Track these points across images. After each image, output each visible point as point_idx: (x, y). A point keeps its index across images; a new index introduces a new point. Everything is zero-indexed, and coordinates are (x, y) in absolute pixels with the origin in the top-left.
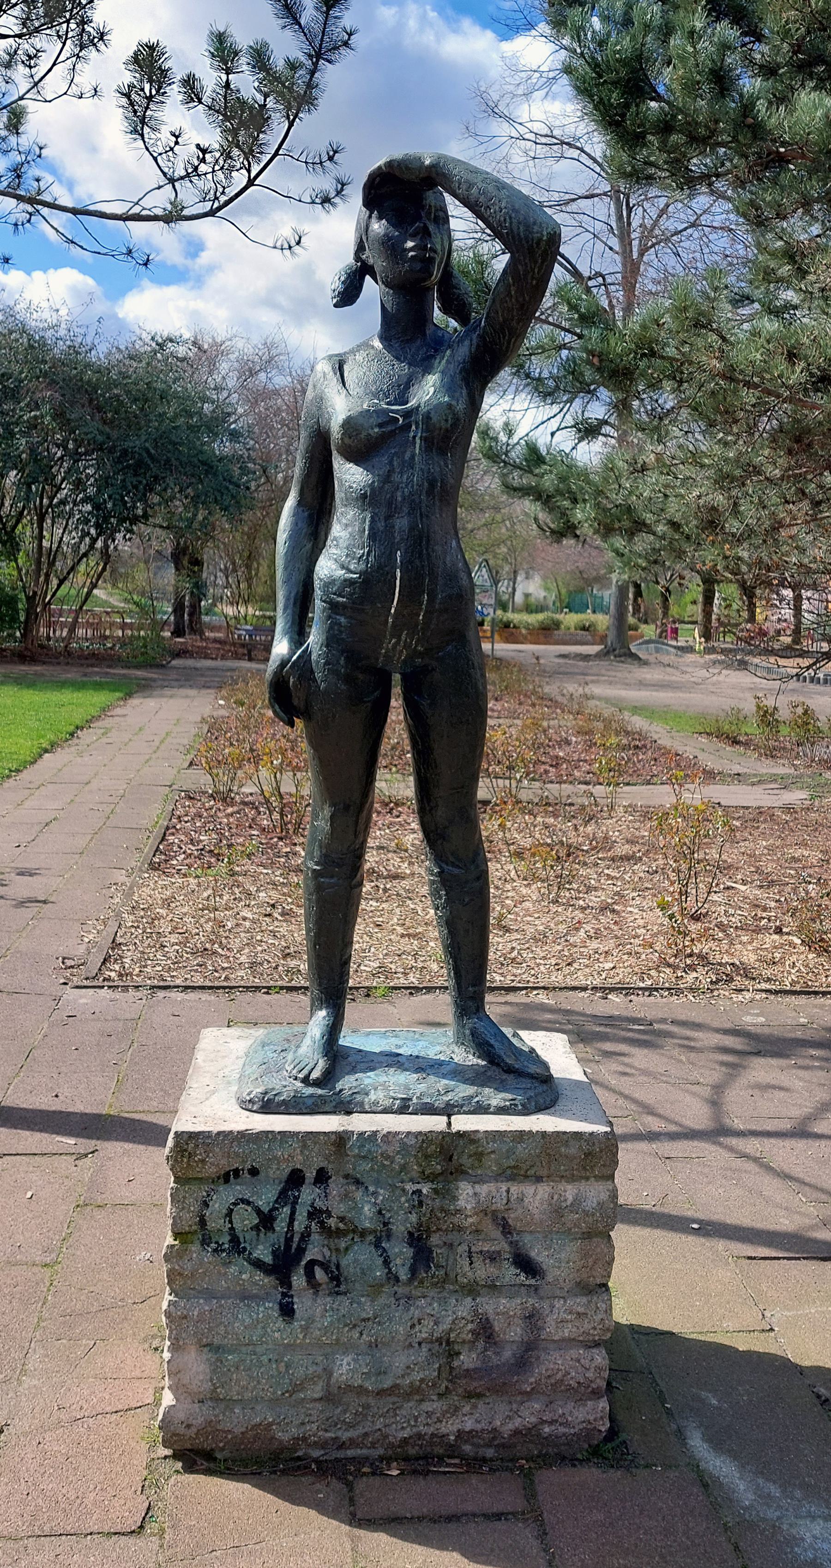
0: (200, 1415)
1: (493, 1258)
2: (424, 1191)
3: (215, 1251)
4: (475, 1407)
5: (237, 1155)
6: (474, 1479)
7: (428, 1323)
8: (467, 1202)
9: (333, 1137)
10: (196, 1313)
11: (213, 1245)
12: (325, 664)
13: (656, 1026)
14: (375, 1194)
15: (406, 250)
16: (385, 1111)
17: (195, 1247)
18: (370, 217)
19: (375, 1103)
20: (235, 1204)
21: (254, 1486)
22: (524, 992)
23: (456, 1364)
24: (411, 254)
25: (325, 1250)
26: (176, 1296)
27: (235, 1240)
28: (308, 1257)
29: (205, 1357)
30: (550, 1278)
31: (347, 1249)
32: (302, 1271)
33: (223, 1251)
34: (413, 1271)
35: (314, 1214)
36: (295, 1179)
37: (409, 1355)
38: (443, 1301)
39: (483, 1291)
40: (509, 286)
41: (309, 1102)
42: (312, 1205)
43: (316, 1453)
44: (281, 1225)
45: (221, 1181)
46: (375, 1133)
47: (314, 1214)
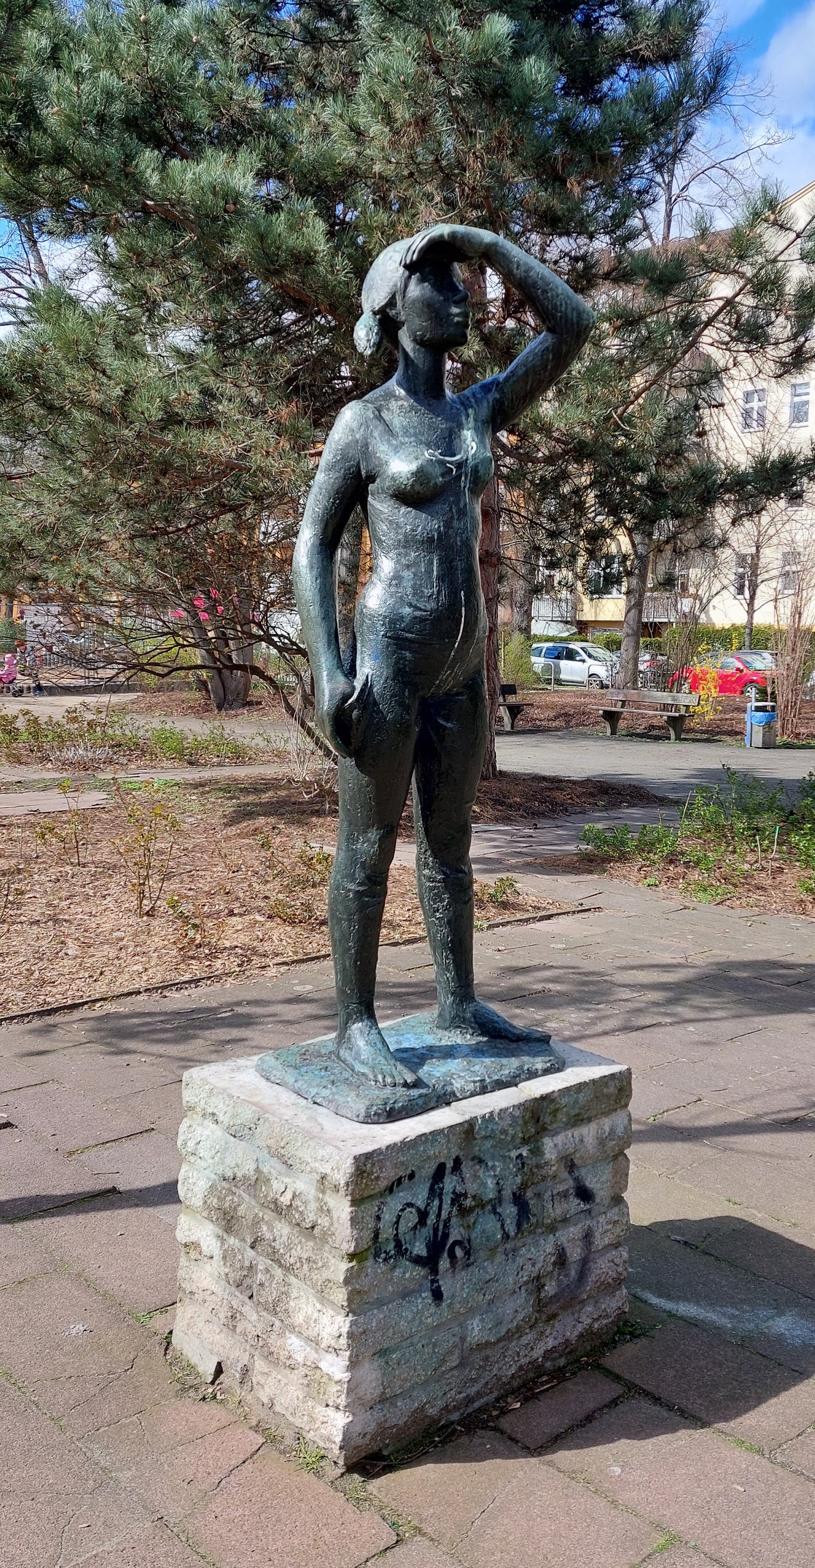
0: (370, 1422)
1: (565, 1195)
2: (525, 1154)
3: (385, 1260)
4: (553, 1326)
5: (402, 1163)
6: (569, 1385)
7: (528, 1267)
8: (551, 1153)
9: (466, 1125)
10: (374, 1324)
11: (383, 1255)
12: (392, 696)
13: (239, 1010)
14: (493, 1167)
15: (451, 314)
16: (473, 1095)
17: (370, 1263)
18: (409, 277)
19: (462, 1090)
20: (402, 1210)
21: (435, 1462)
22: (86, 1007)
23: (543, 1295)
24: (456, 319)
25: (462, 1229)
26: (355, 1314)
27: (398, 1244)
28: (451, 1241)
29: (376, 1364)
30: (598, 1200)
31: (474, 1223)
32: (446, 1255)
33: (391, 1257)
34: (519, 1226)
35: (457, 1198)
36: (439, 1173)
37: (515, 1301)
38: (536, 1244)
39: (559, 1225)
40: (548, 360)
41: (420, 1101)
42: (454, 1192)
43: (455, 1416)
44: (431, 1219)
45: (387, 1192)
46: (491, 1113)
47: (457, 1198)
